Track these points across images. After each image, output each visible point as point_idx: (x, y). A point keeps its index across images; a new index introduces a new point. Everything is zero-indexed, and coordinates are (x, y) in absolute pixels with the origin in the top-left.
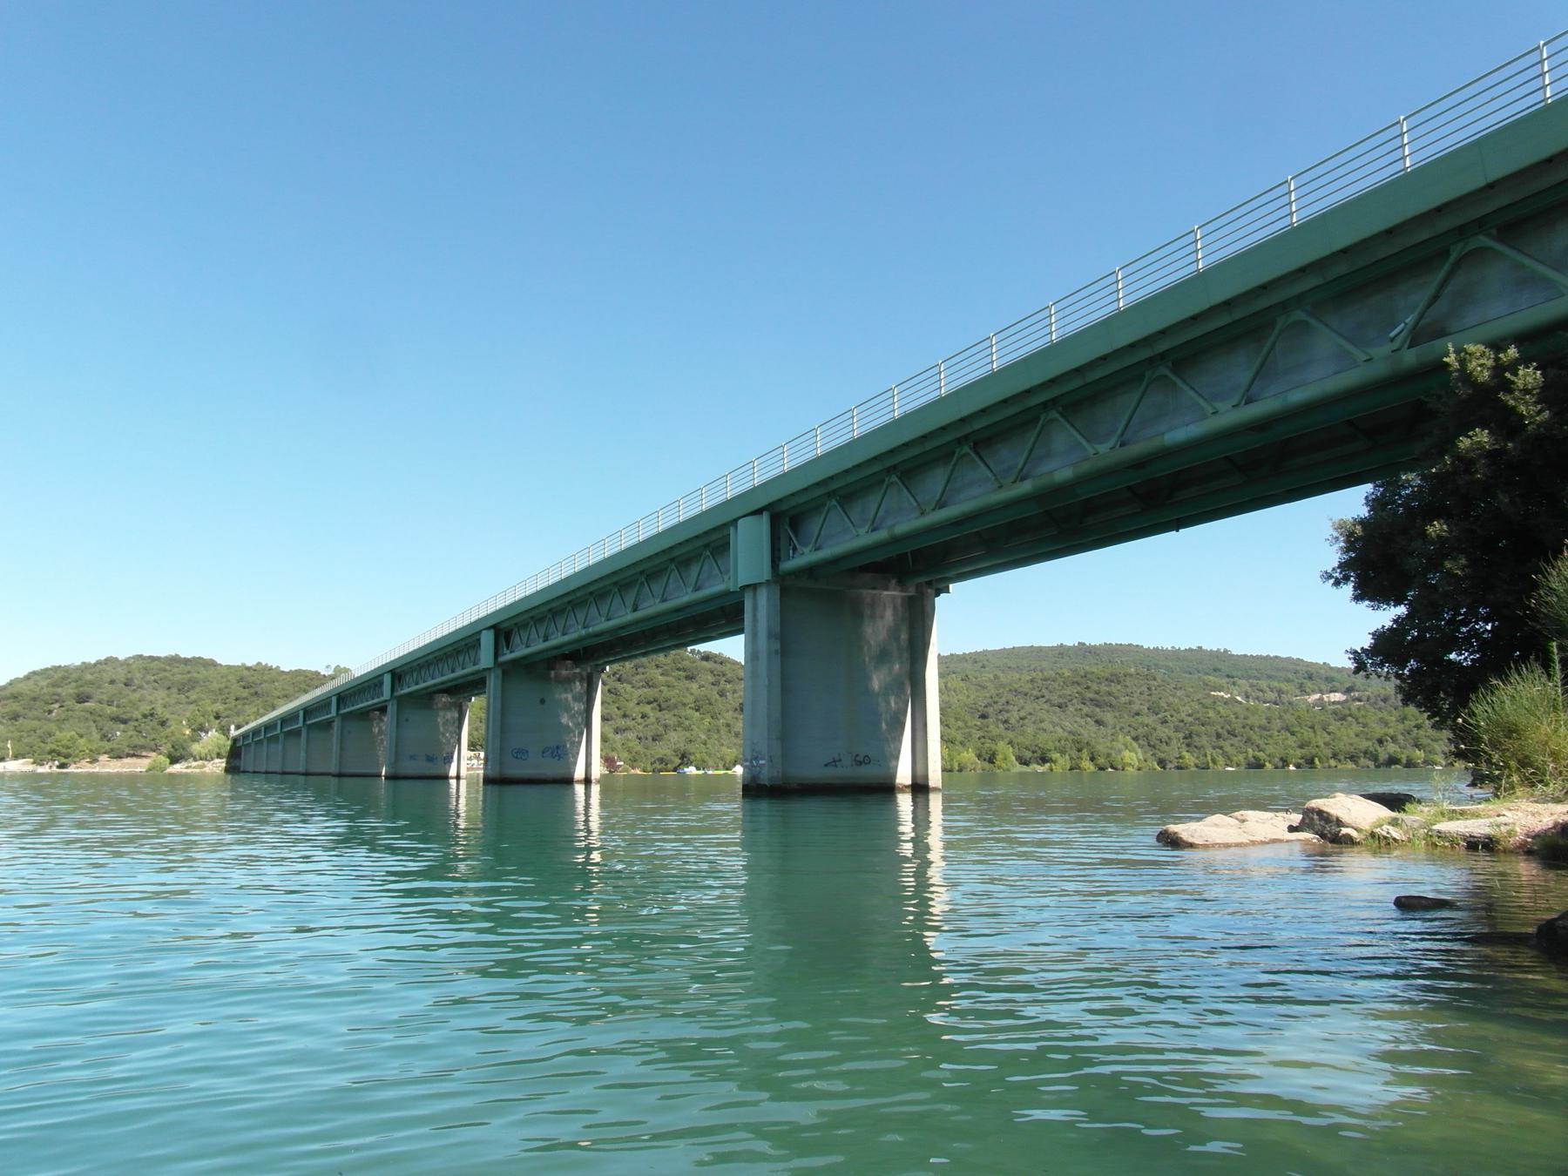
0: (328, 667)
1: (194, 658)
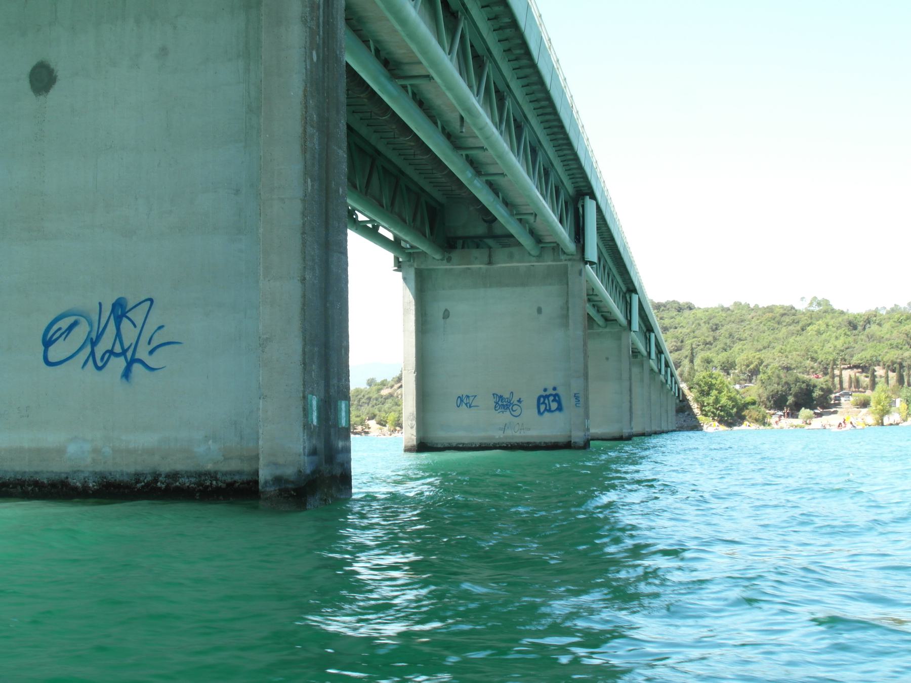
0: (802, 299)
1: (668, 303)
